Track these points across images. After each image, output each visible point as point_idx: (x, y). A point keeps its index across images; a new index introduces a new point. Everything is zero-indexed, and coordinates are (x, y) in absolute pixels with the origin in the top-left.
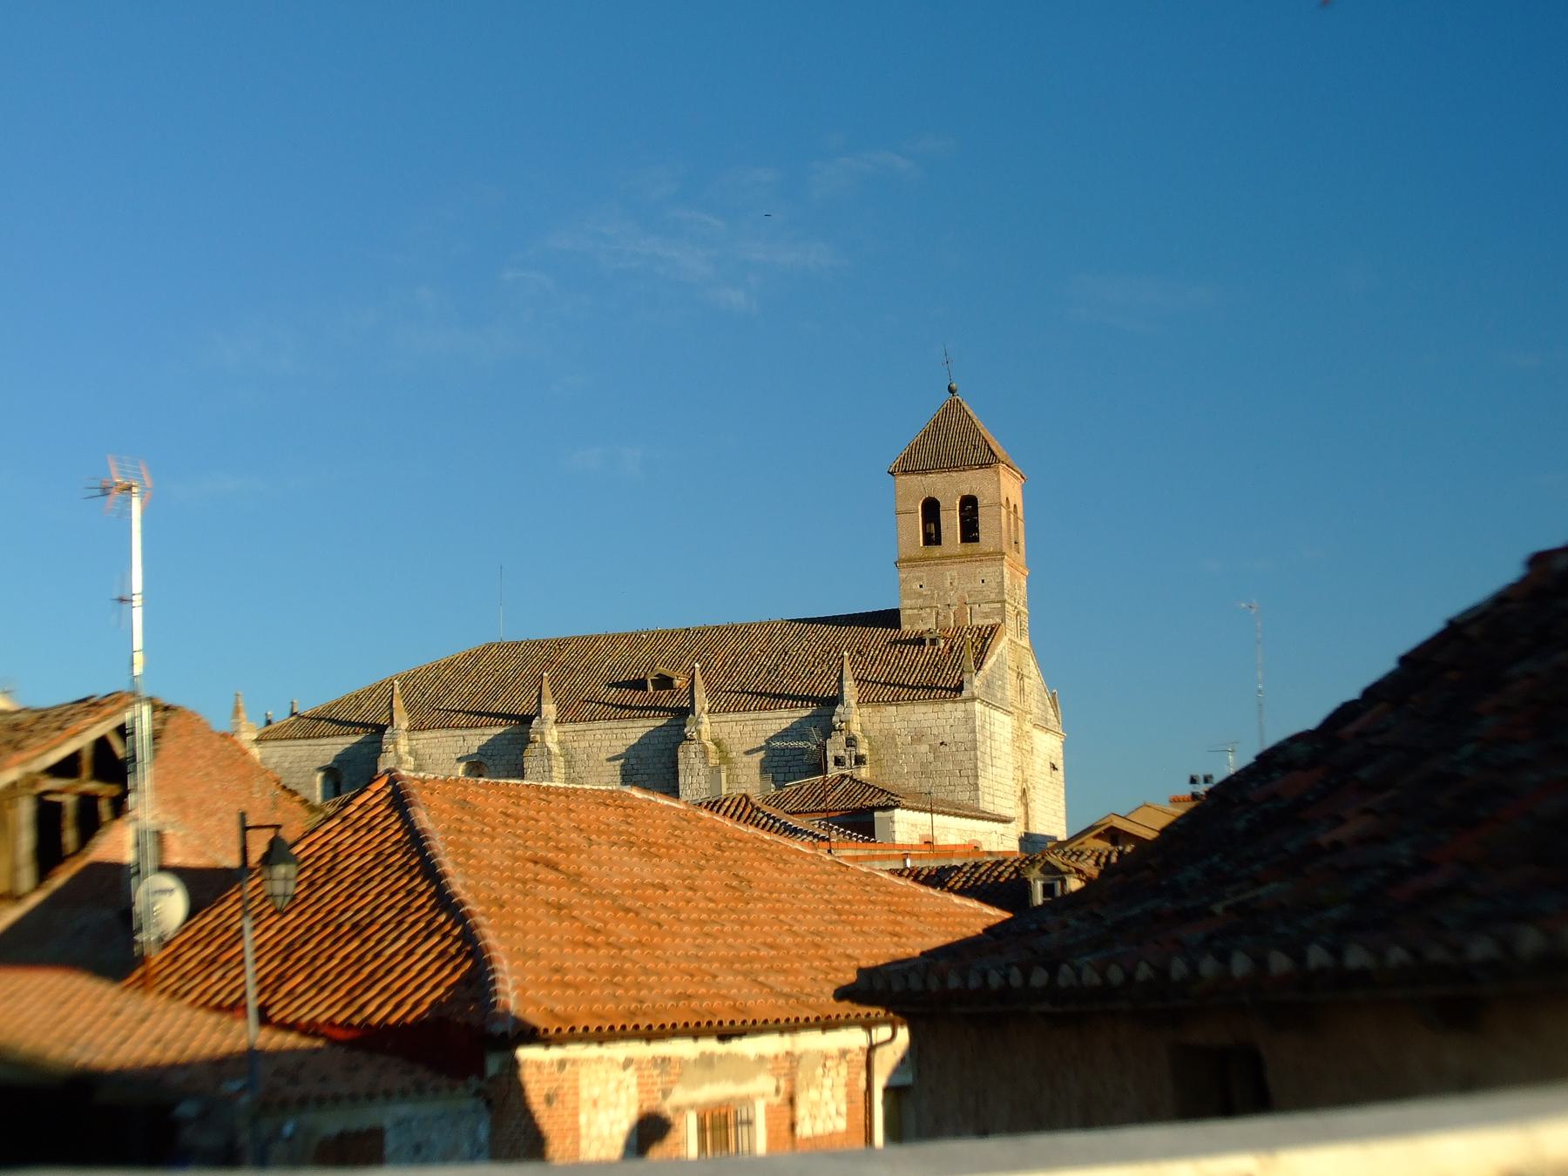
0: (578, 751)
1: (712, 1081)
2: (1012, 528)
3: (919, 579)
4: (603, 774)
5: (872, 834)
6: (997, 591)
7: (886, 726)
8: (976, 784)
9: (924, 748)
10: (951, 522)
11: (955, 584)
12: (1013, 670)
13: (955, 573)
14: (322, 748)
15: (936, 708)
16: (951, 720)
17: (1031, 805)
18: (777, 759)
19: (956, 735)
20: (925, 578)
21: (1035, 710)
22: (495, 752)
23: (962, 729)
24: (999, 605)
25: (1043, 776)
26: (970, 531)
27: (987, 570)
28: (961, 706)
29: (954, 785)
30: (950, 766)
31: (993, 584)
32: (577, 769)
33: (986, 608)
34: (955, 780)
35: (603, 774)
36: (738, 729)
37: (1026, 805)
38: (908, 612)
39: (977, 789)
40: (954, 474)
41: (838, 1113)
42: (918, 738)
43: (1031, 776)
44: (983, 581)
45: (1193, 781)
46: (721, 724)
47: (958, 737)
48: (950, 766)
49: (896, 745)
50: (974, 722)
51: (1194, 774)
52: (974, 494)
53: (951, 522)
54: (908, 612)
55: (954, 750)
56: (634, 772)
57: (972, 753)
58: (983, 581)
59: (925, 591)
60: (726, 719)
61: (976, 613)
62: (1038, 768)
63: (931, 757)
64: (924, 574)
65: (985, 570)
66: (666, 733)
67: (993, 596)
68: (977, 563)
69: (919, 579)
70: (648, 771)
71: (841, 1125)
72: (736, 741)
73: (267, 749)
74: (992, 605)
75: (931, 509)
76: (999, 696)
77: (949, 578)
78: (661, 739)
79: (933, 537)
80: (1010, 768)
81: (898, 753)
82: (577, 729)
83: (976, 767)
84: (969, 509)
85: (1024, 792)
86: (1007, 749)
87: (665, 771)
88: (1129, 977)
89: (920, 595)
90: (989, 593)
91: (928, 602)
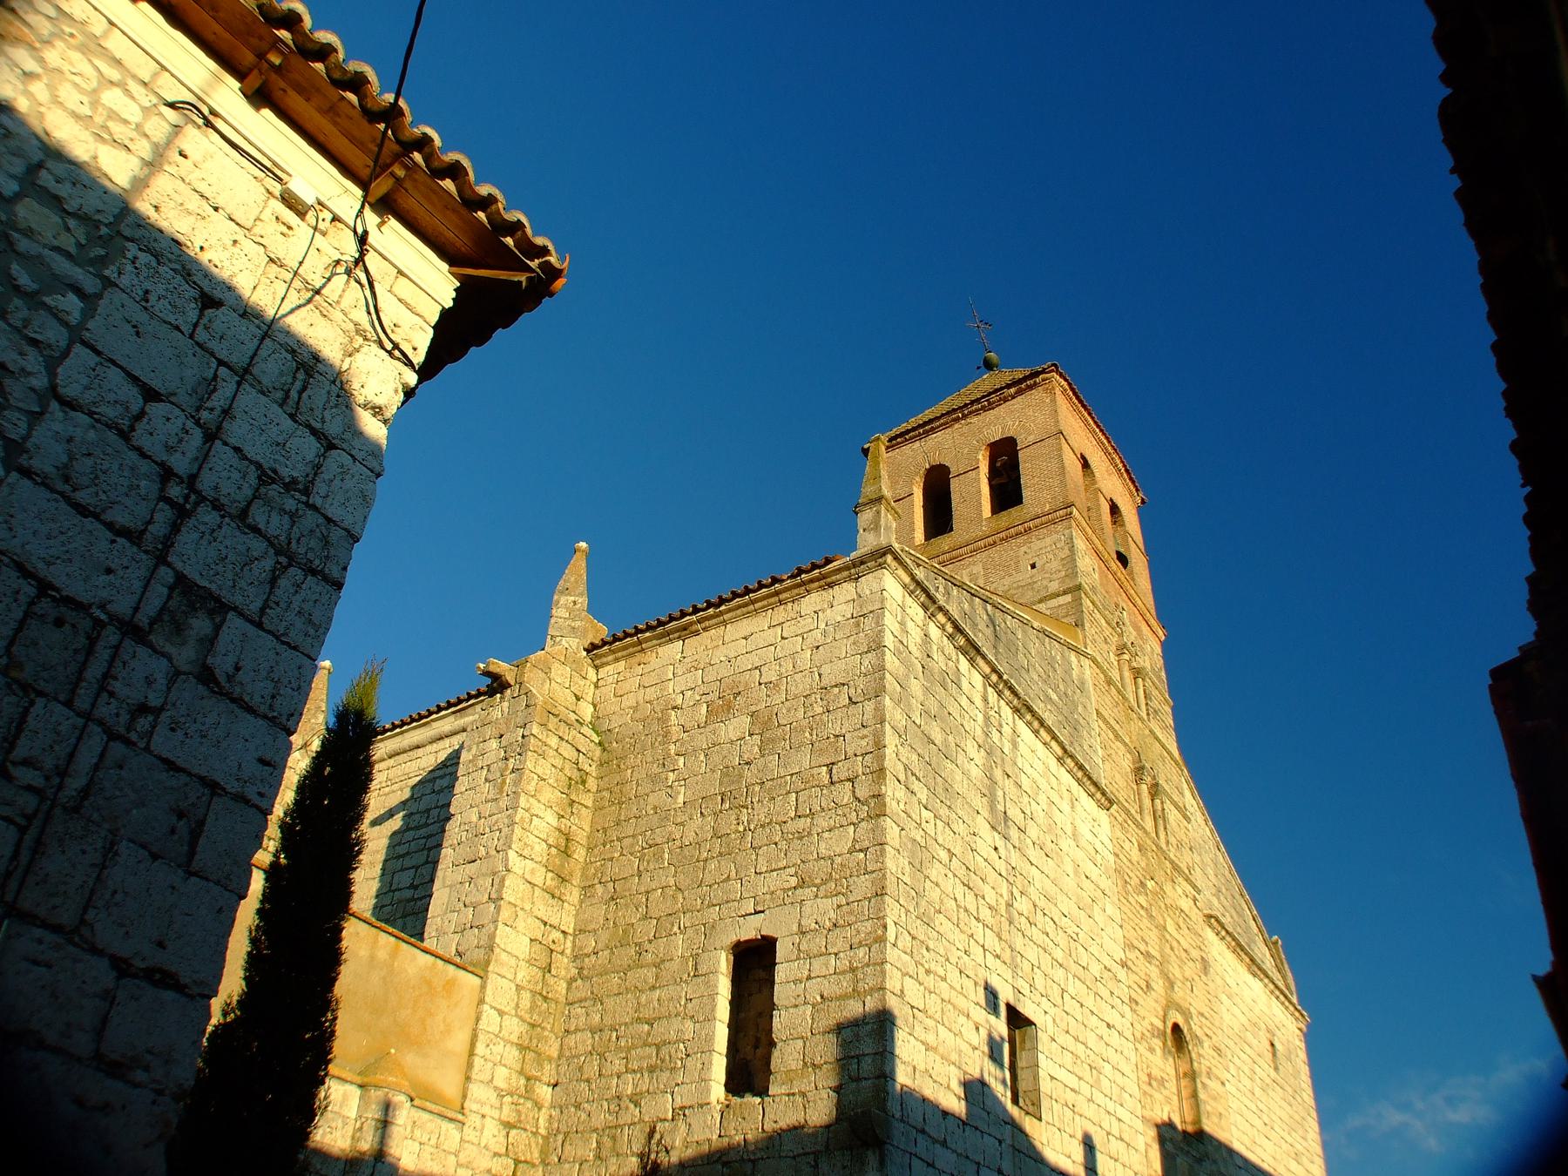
5: (420, 936)
8: (878, 796)
9: (737, 726)
15: (780, 614)
16: (817, 634)
19: (825, 670)
23: (844, 647)
26: (1006, 492)
27: (1044, 546)
28: (846, 591)
29: (812, 814)
34: (815, 799)
40: (974, 420)
42: (721, 708)
43: (1217, 1050)
44: (1033, 566)
48: (803, 760)
49: (667, 734)
50: (879, 622)
55: (819, 710)
57: (869, 706)
63: (752, 746)
65: (1039, 544)
67: (1054, 586)
68: (1020, 540)
74: (1054, 603)
81: (667, 756)
88: (236, 1015)
90: (1045, 582)
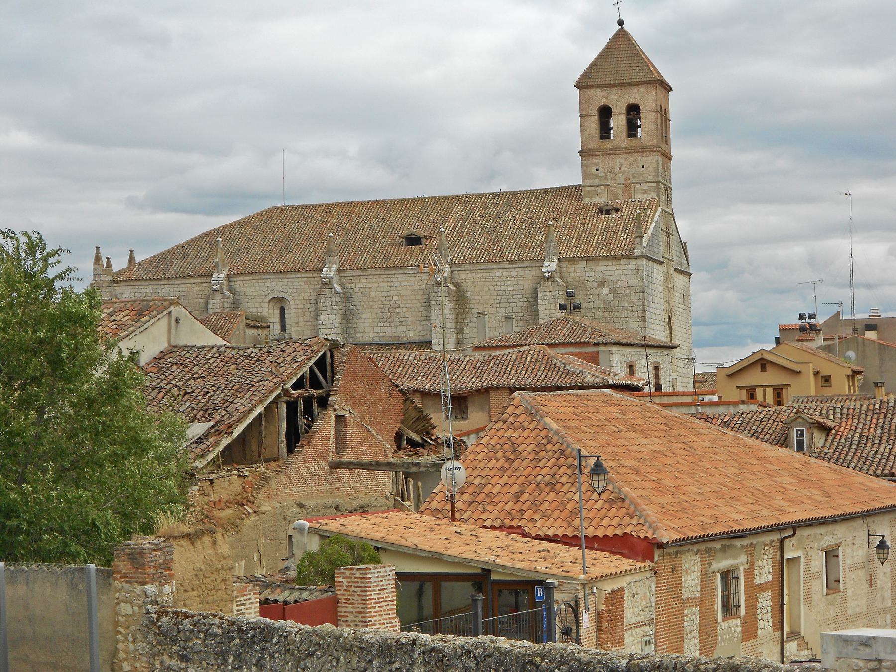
0: (356, 290)
1: (726, 558)
2: (663, 126)
3: (596, 164)
4: (374, 307)
6: (653, 174)
7: (579, 275)
9: (605, 291)
10: (618, 123)
11: (623, 168)
12: (664, 231)
13: (622, 161)
14: (162, 287)
17: (673, 327)
18: (500, 297)
20: (600, 164)
21: (676, 258)
22: (294, 291)
24: (654, 184)
25: (680, 305)
30: (624, 304)
31: (651, 169)
32: (355, 303)
33: (645, 186)
35: (374, 307)
36: (471, 275)
37: (670, 328)
38: (588, 189)
39: (644, 320)
41: (769, 573)
45: (802, 317)
46: (459, 272)
47: (631, 283)
51: (802, 312)
52: (638, 103)
53: (618, 123)
54: (588, 189)
56: (397, 306)
57: (641, 295)
58: (643, 167)
59: (601, 173)
60: (463, 269)
61: (637, 190)
62: (677, 299)
63: (611, 297)
64: (600, 161)
66: (420, 278)
67: (650, 178)
69: (596, 164)
70: (407, 305)
71: (770, 578)
72: (470, 284)
73: (121, 288)
75: (605, 113)
76: (656, 251)
77: (618, 164)
78: (416, 283)
79: (605, 132)
80: (662, 302)
82: (354, 274)
83: (644, 305)
84: (633, 114)
85: (669, 318)
86: (660, 288)
87: (419, 305)
89: (597, 176)
90: (647, 175)
91: (602, 182)
